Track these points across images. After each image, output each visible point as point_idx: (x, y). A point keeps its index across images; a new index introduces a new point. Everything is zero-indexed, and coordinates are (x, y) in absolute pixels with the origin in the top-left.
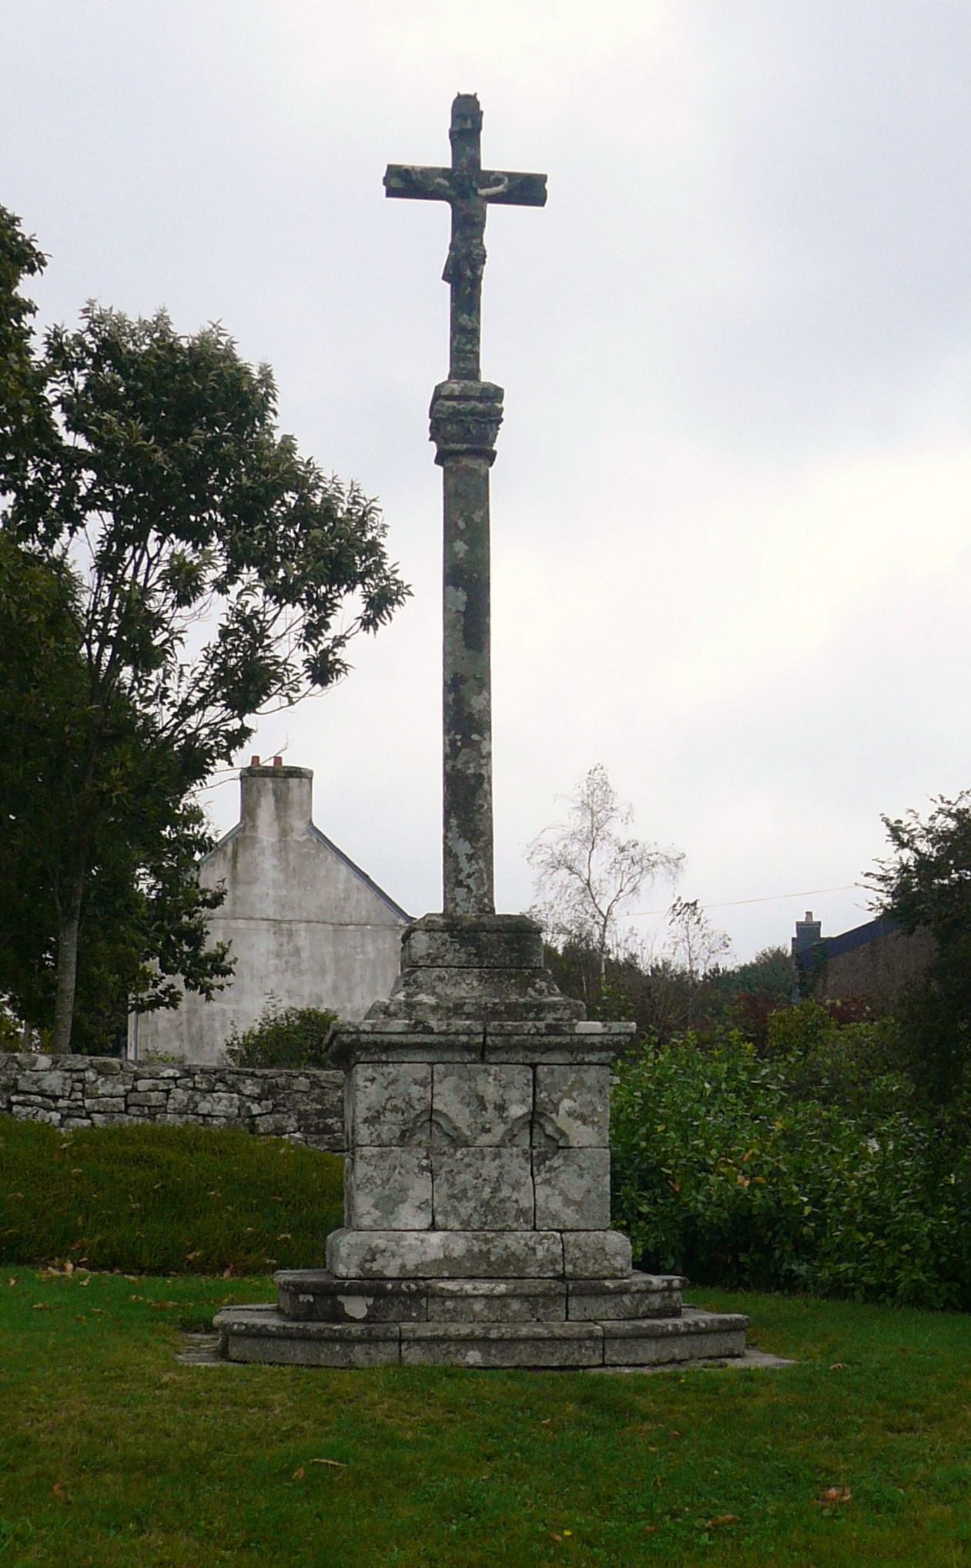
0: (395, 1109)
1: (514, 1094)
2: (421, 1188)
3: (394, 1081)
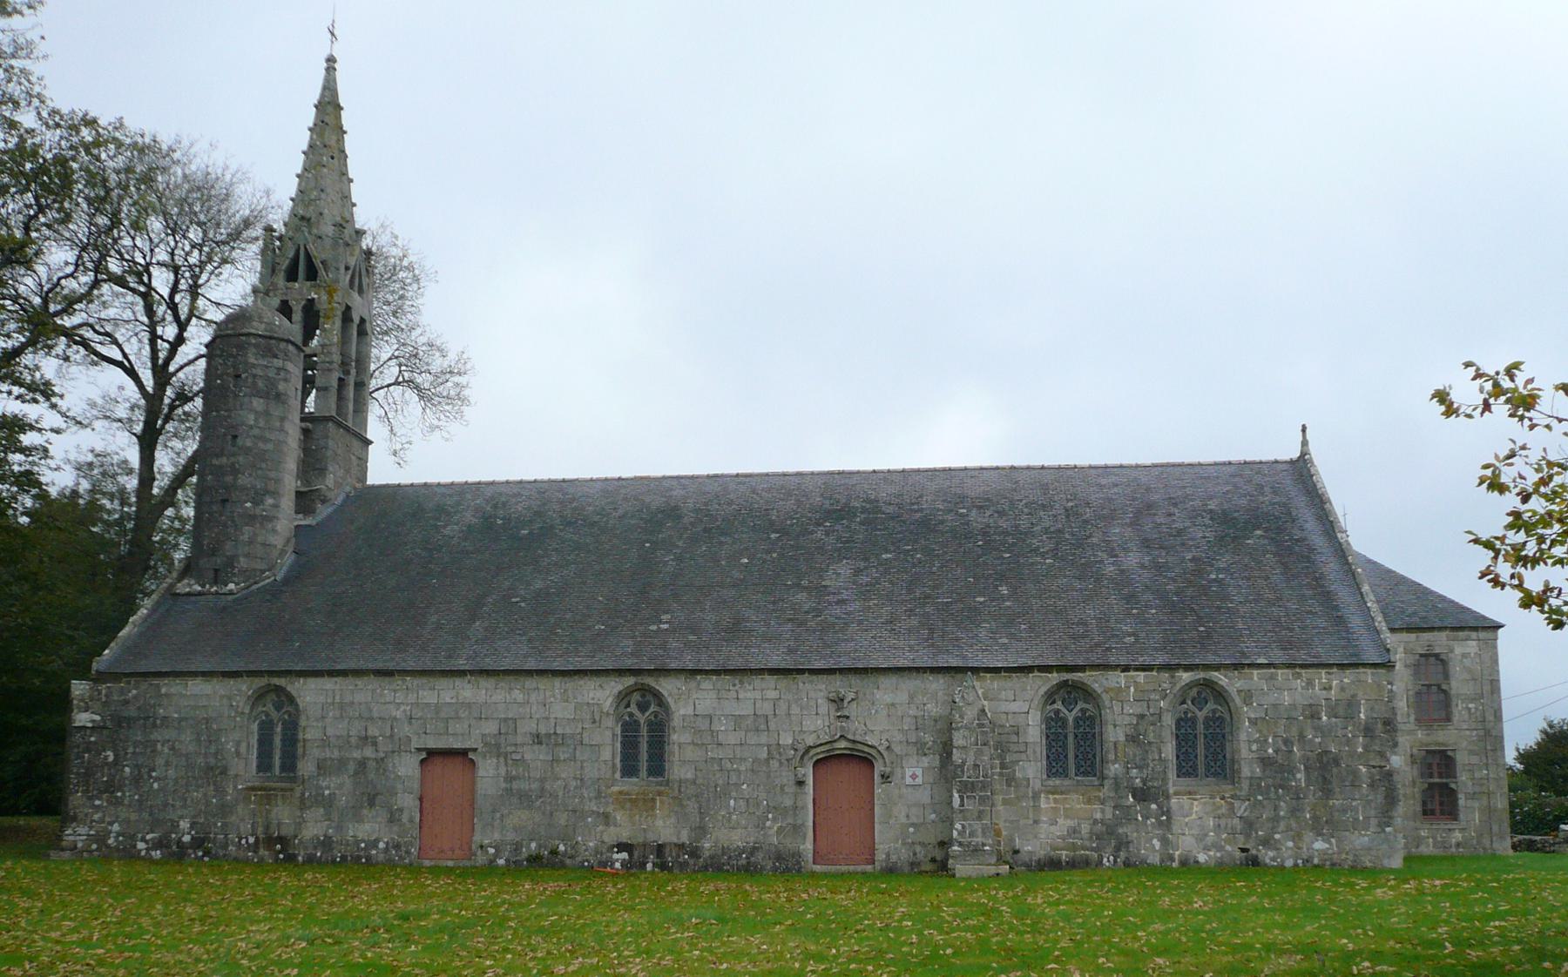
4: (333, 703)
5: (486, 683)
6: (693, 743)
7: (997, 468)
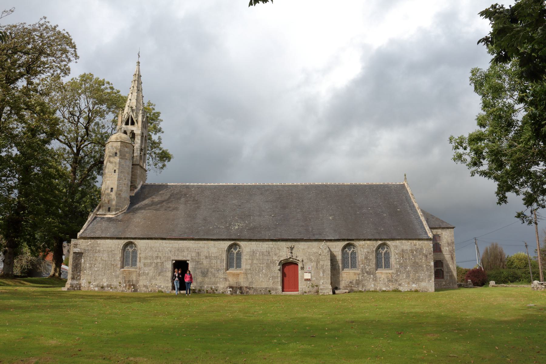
4: (148, 247)
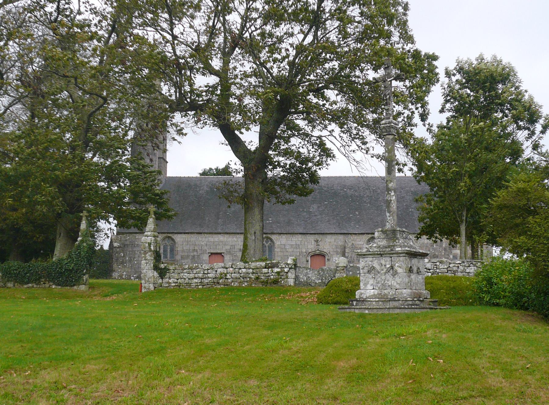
0: (367, 267)
1: (388, 263)
2: (371, 281)
3: (366, 261)
5: (226, 236)
6: (280, 251)
7: (354, 177)
